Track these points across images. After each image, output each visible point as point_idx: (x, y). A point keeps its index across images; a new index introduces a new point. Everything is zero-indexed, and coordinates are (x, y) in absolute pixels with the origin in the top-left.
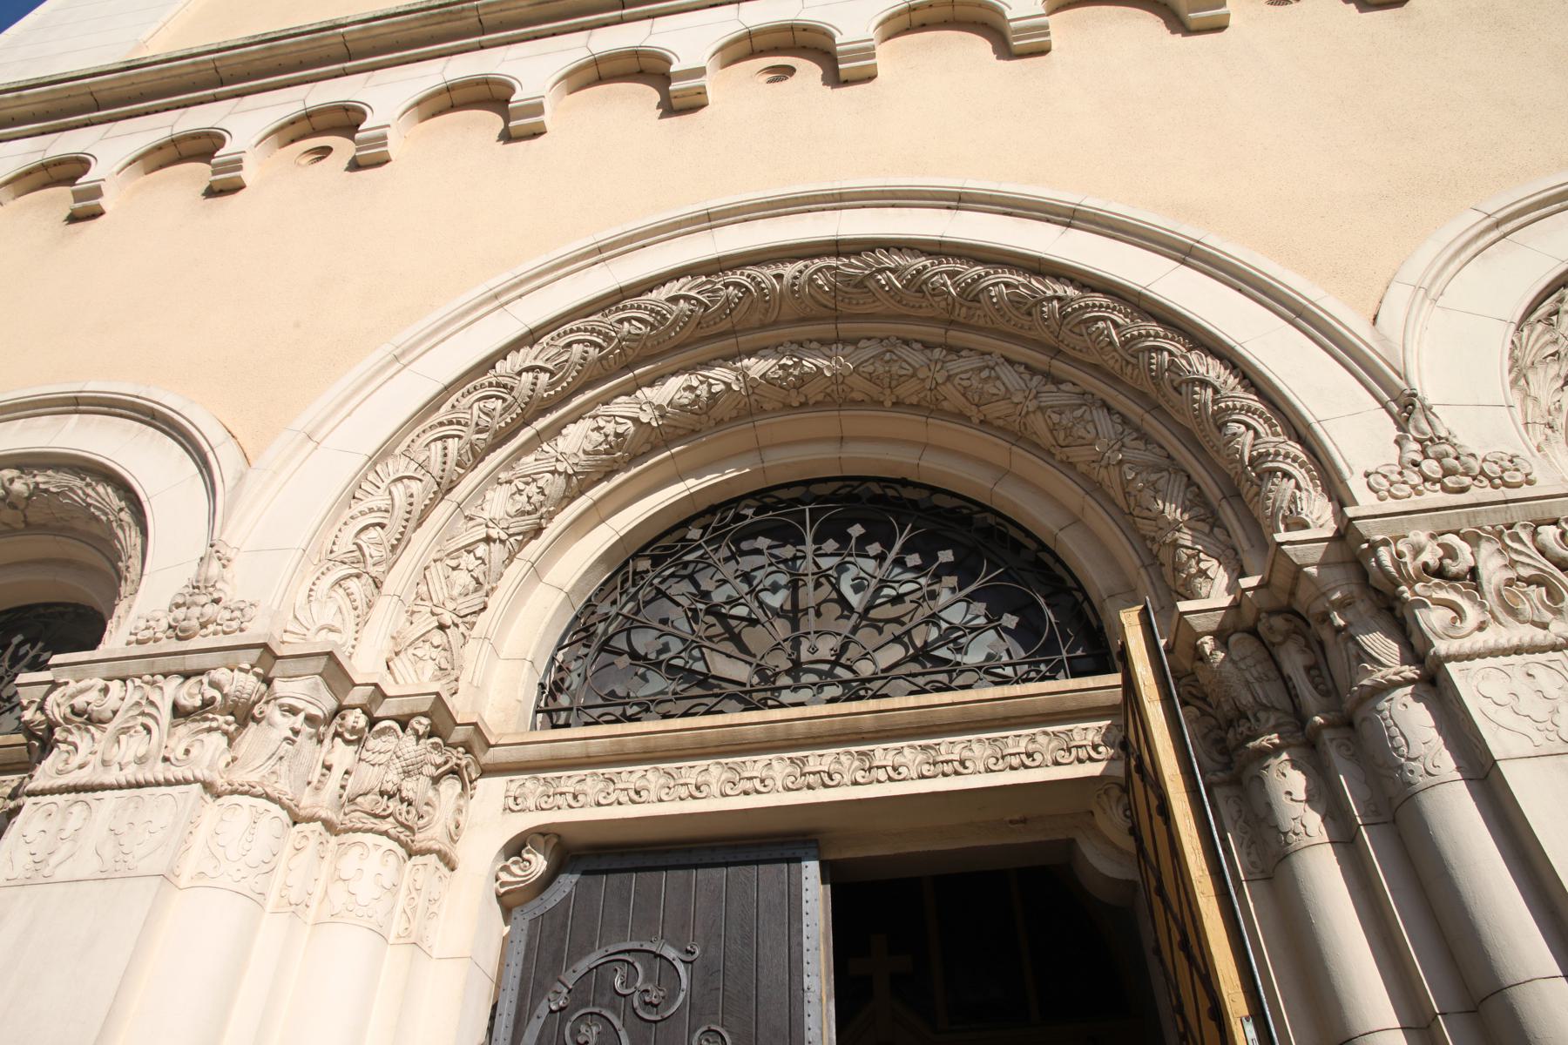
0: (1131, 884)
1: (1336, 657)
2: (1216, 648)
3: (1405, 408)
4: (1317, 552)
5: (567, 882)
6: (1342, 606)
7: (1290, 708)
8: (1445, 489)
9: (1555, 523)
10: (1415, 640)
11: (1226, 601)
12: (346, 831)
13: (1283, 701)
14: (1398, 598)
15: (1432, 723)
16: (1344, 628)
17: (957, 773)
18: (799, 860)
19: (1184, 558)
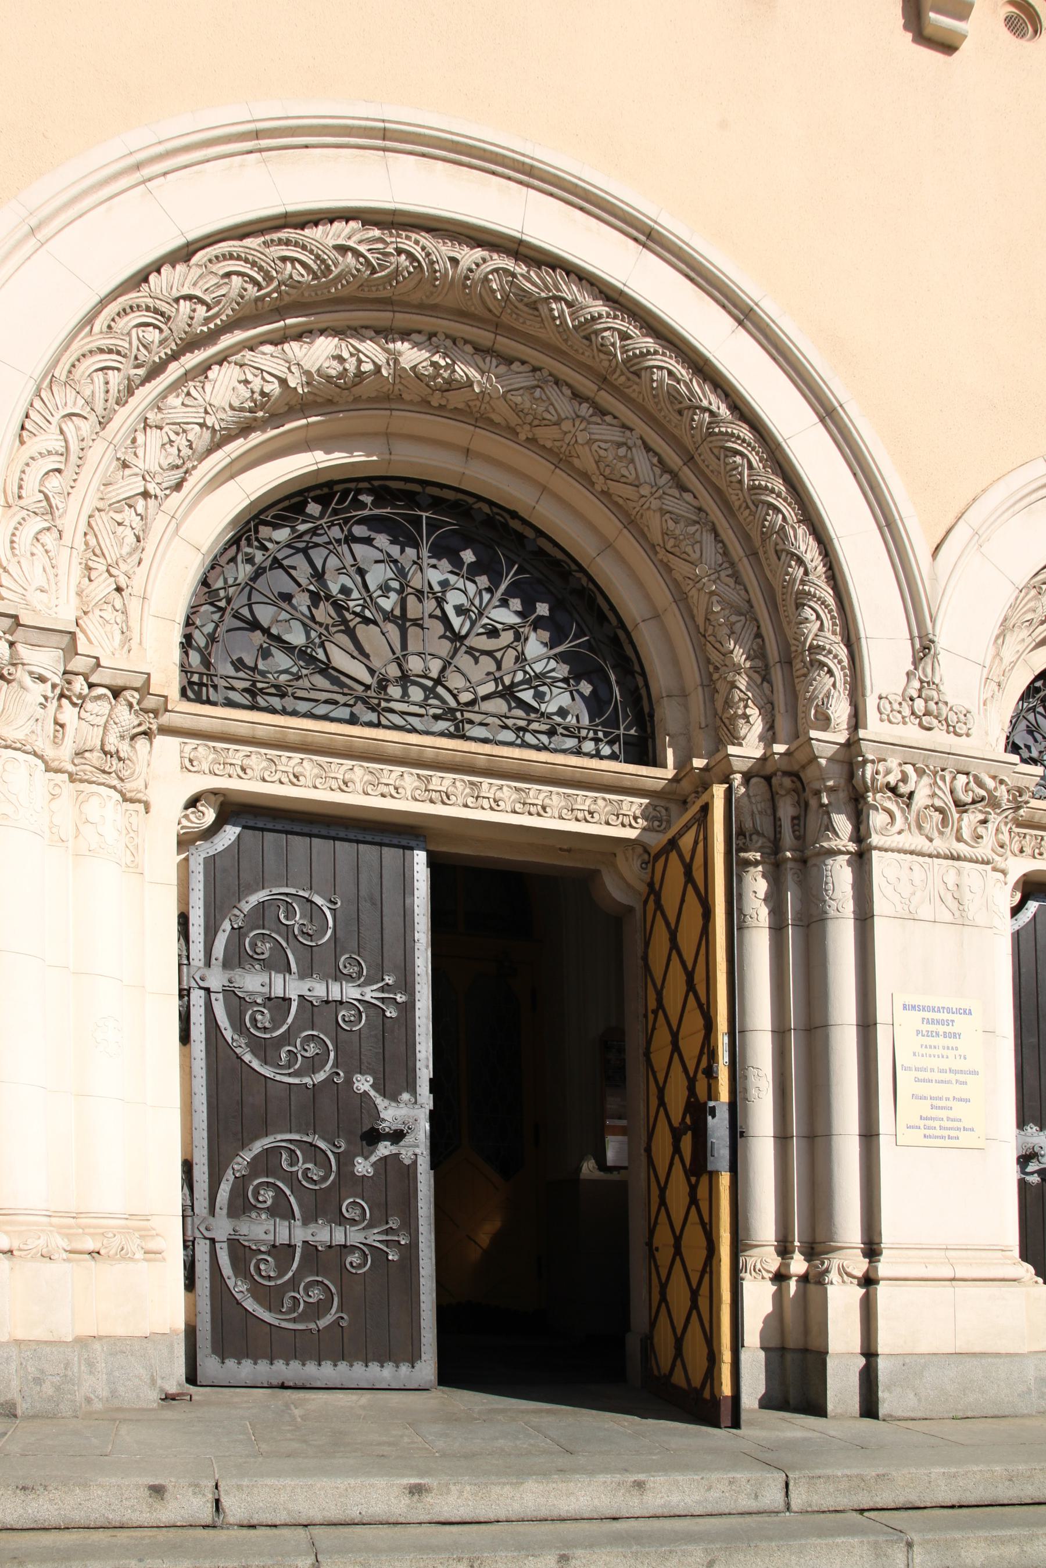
0: (630, 909)
1: (813, 821)
2: (742, 784)
3: (924, 649)
4: (830, 750)
5: (230, 833)
6: (831, 790)
7: (771, 836)
8: (921, 725)
9: (967, 774)
10: (862, 828)
11: (758, 753)
12: (82, 781)
13: (769, 830)
14: (865, 798)
15: (851, 881)
16: (826, 806)
17: (539, 815)
18: (412, 849)
19: (737, 699)
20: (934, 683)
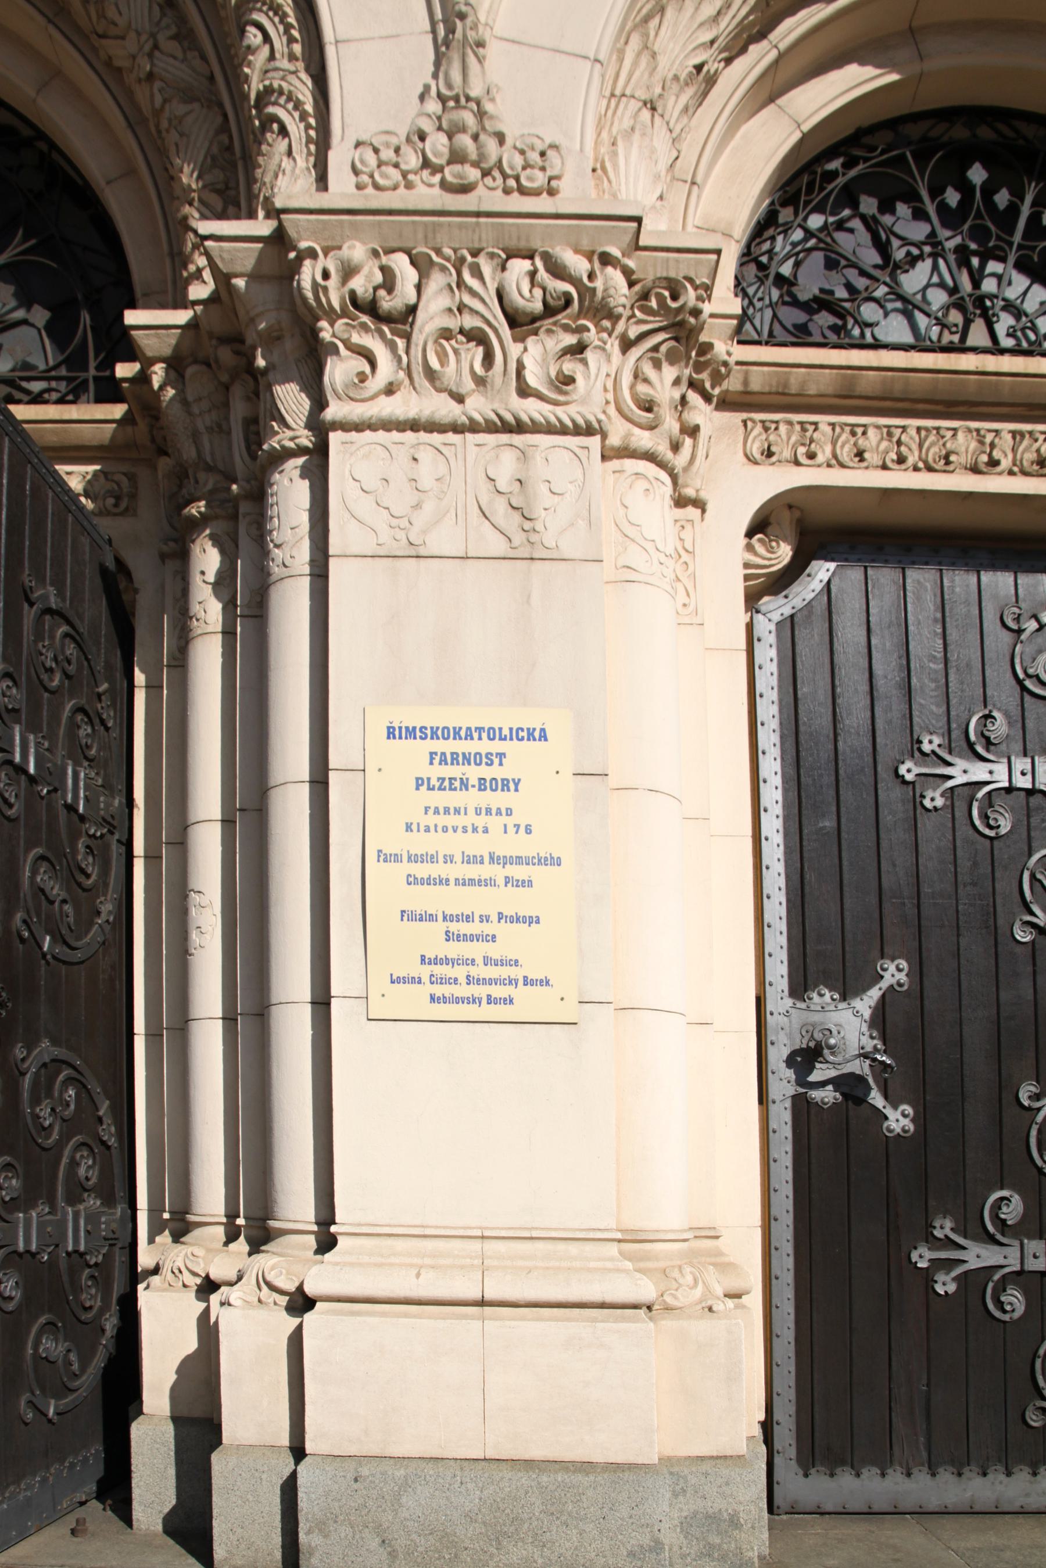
5: (822, 571)
8: (444, 185)
15: (308, 506)
20: (468, 99)
